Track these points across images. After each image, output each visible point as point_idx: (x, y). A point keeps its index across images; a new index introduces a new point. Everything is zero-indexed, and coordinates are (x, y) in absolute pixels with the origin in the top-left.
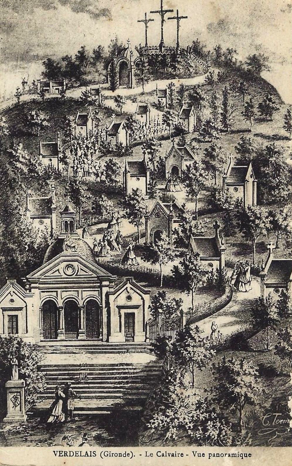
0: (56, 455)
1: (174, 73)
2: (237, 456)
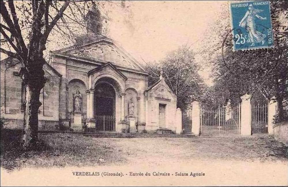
0: (74, 174)
1: (283, 37)
2: (201, 175)
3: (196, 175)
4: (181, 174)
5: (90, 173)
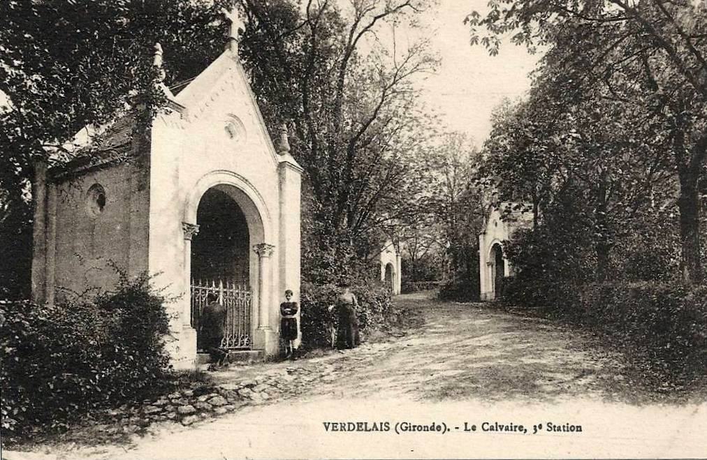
0: (327, 429)
3: (418, 429)
4: (511, 427)
5: (366, 423)
